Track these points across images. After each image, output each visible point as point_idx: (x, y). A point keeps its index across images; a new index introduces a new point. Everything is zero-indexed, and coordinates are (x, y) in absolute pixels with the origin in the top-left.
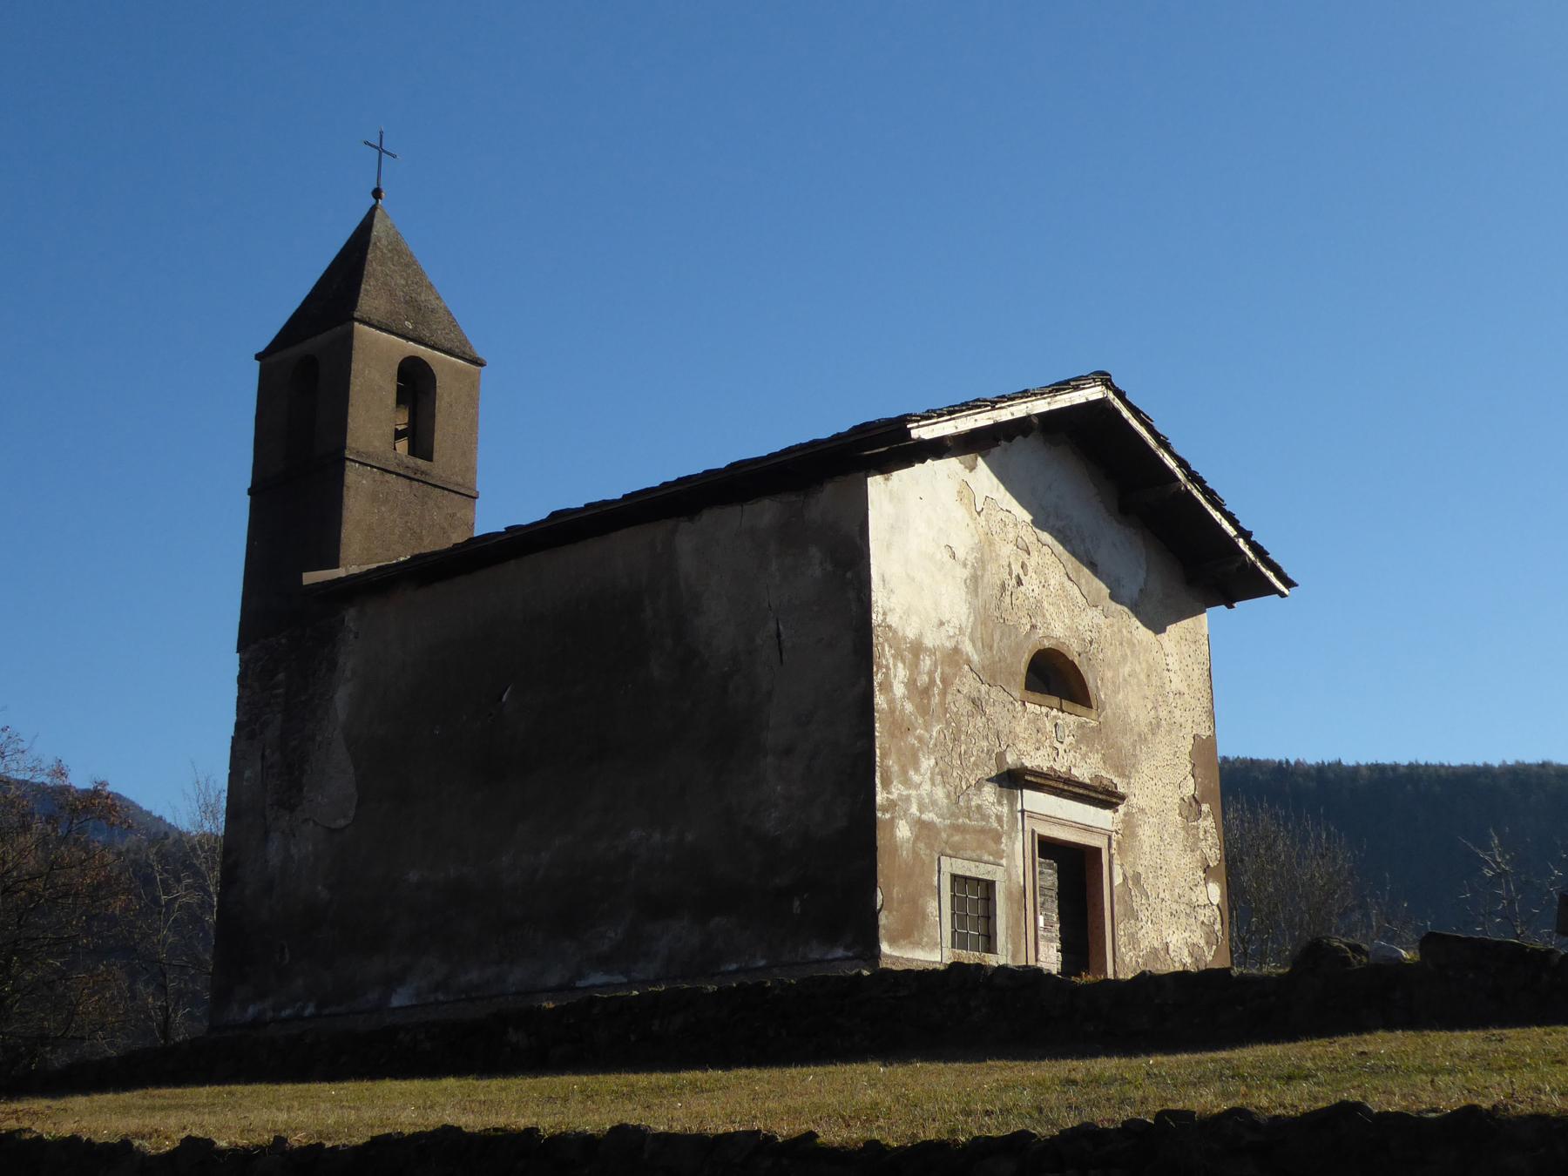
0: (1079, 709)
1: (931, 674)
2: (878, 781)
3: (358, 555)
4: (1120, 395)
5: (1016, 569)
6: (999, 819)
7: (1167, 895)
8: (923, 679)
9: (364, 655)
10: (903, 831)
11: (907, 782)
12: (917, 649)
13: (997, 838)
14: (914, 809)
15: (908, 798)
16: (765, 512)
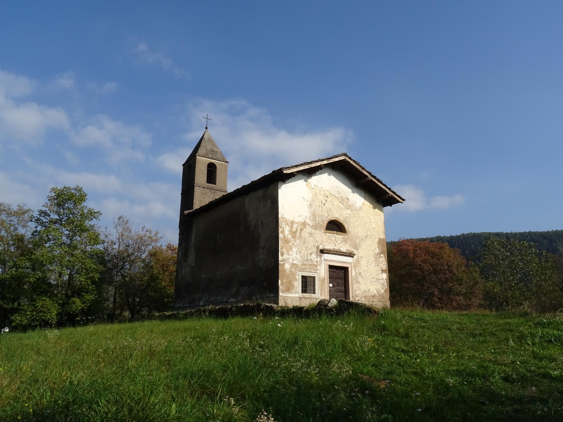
0: (342, 233)
1: (297, 228)
2: (280, 254)
3: (197, 205)
4: (350, 158)
5: (324, 201)
6: (317, 262)
7: (369, 277)
8: (294, 230)
9: (198, 227)
10: (287, 266)
11: (288, 254)
12: (293, 223)
13: (316, 266)
14: (291, 261)
15: (289, 258)
16: (260, 193)
